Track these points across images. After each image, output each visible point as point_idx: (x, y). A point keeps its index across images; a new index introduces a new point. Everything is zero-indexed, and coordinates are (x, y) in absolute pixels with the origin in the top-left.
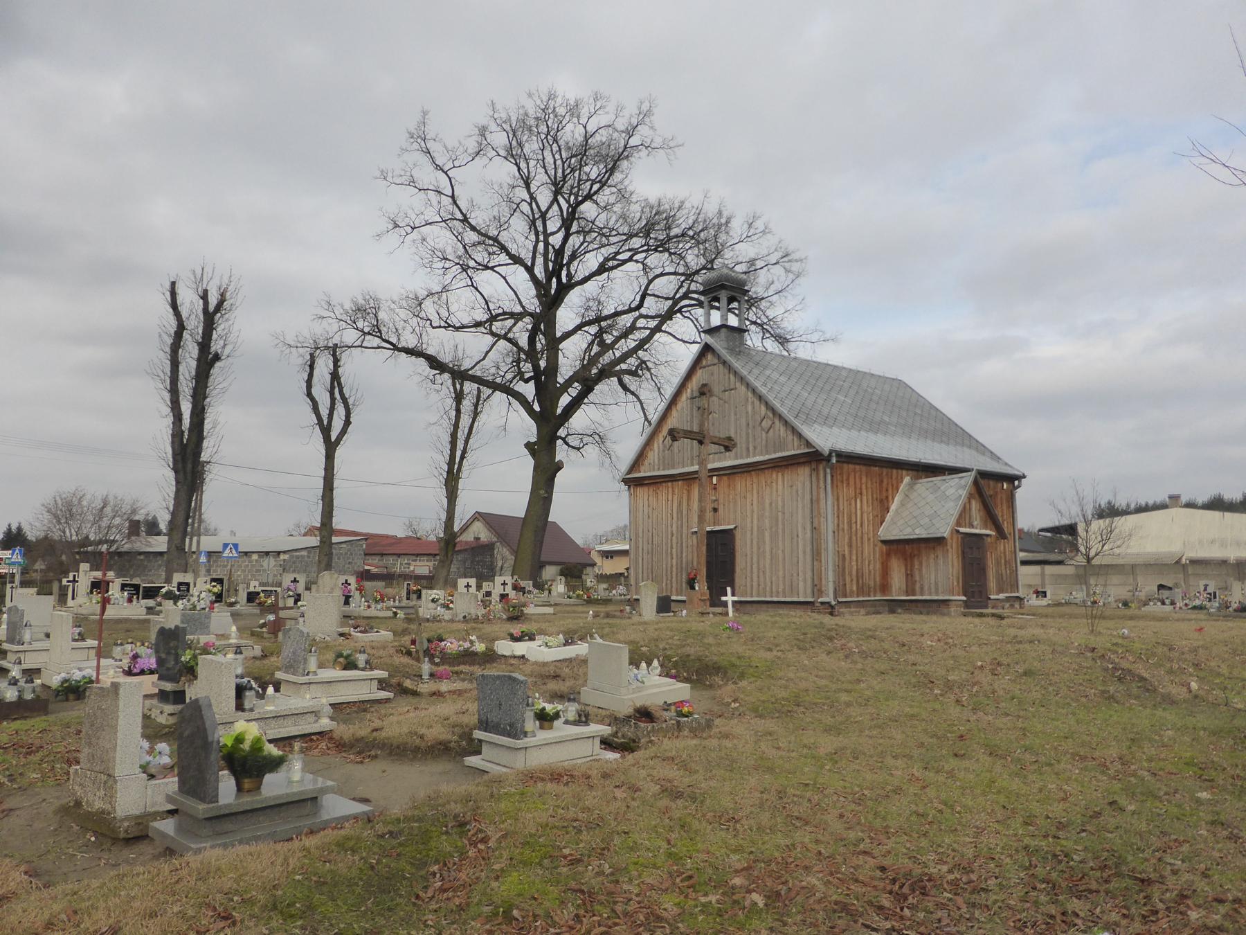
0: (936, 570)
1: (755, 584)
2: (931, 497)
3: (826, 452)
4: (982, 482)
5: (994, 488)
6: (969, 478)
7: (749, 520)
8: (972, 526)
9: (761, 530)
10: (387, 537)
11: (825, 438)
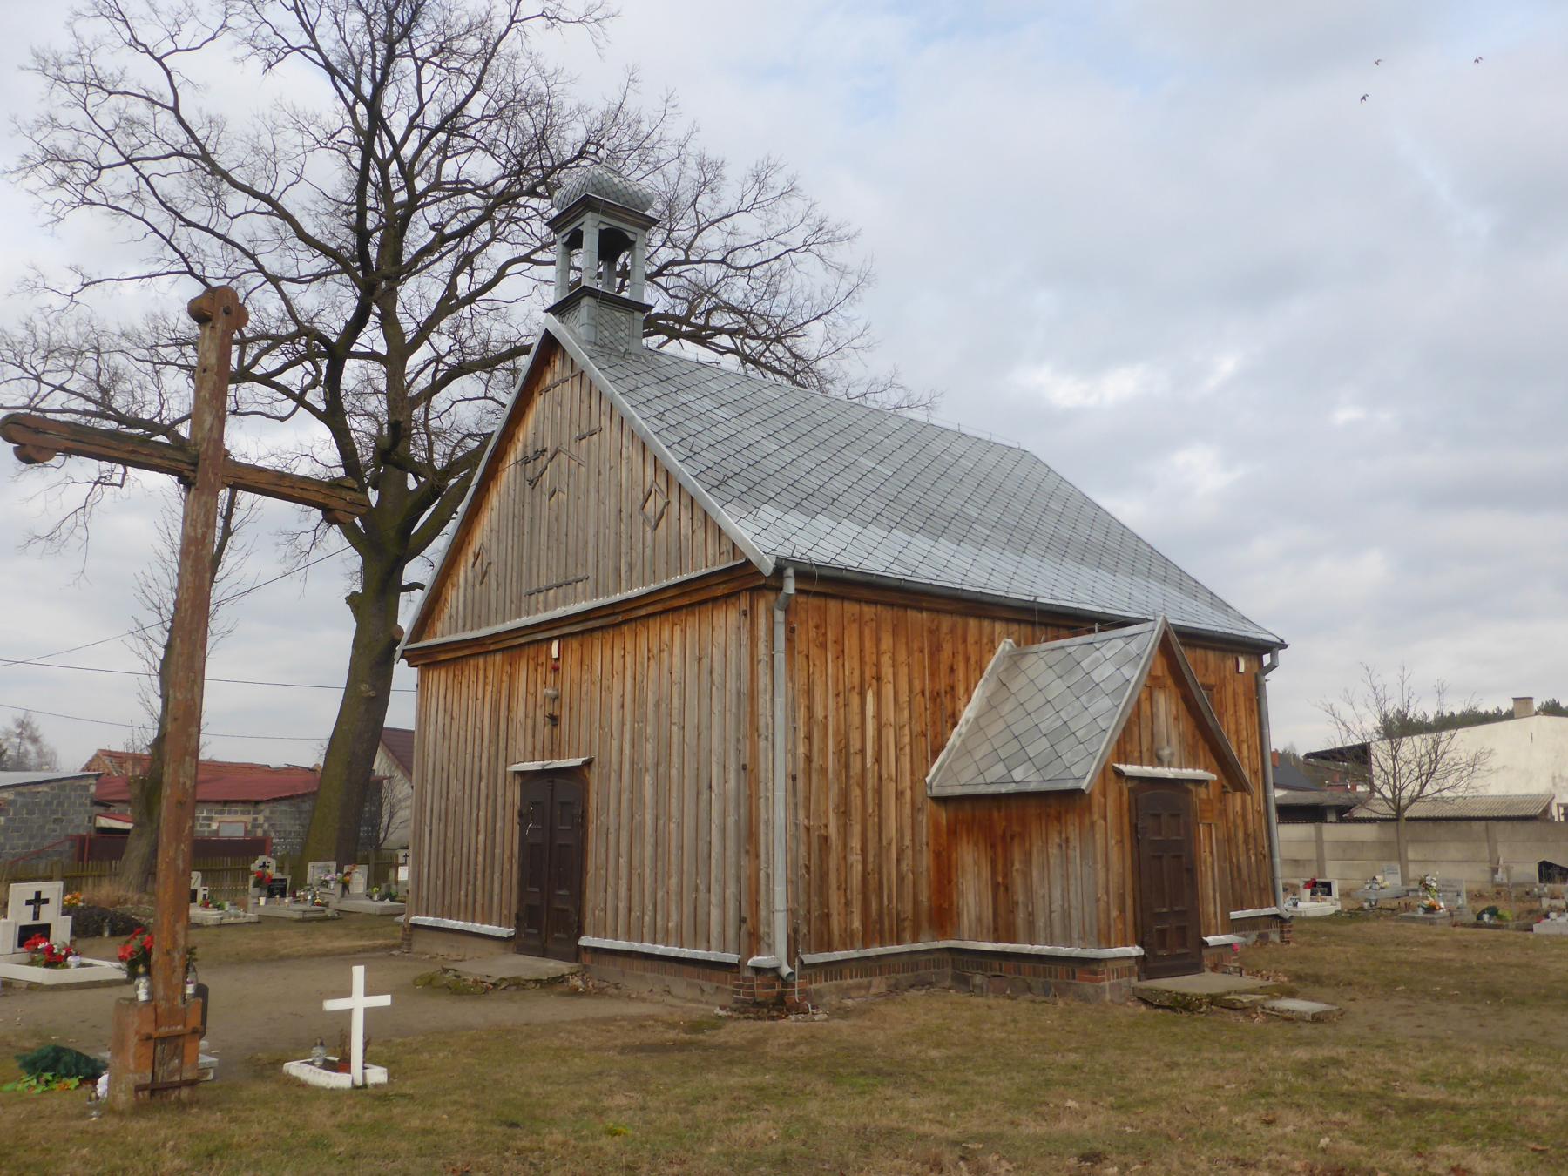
0: (1066, 877)
1: (622, 905)
2: (1057, 688)
3: (768, 566)
4: (1188, 656)
5: (1209, 670)
6: (1144, 641)
7: (615, 744)
8: (1158, 760)
9: (637, 773)
10: (251, 767)
11: (763, 535)
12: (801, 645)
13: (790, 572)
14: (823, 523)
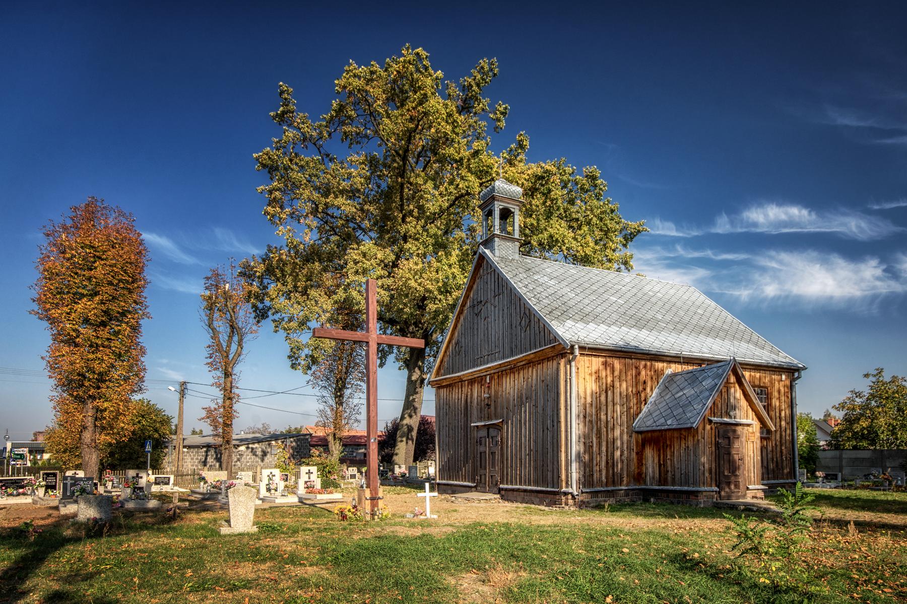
12: (581, 375)
13: (576, 346)
14: (592, 326)
